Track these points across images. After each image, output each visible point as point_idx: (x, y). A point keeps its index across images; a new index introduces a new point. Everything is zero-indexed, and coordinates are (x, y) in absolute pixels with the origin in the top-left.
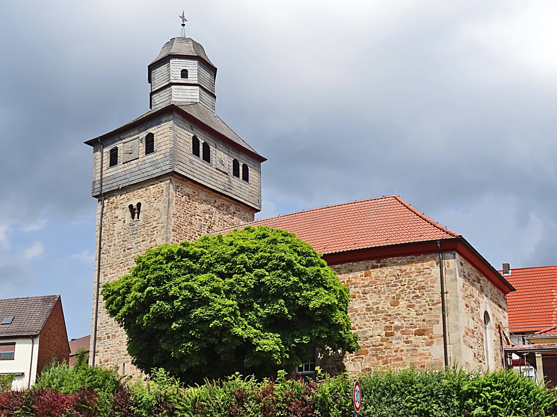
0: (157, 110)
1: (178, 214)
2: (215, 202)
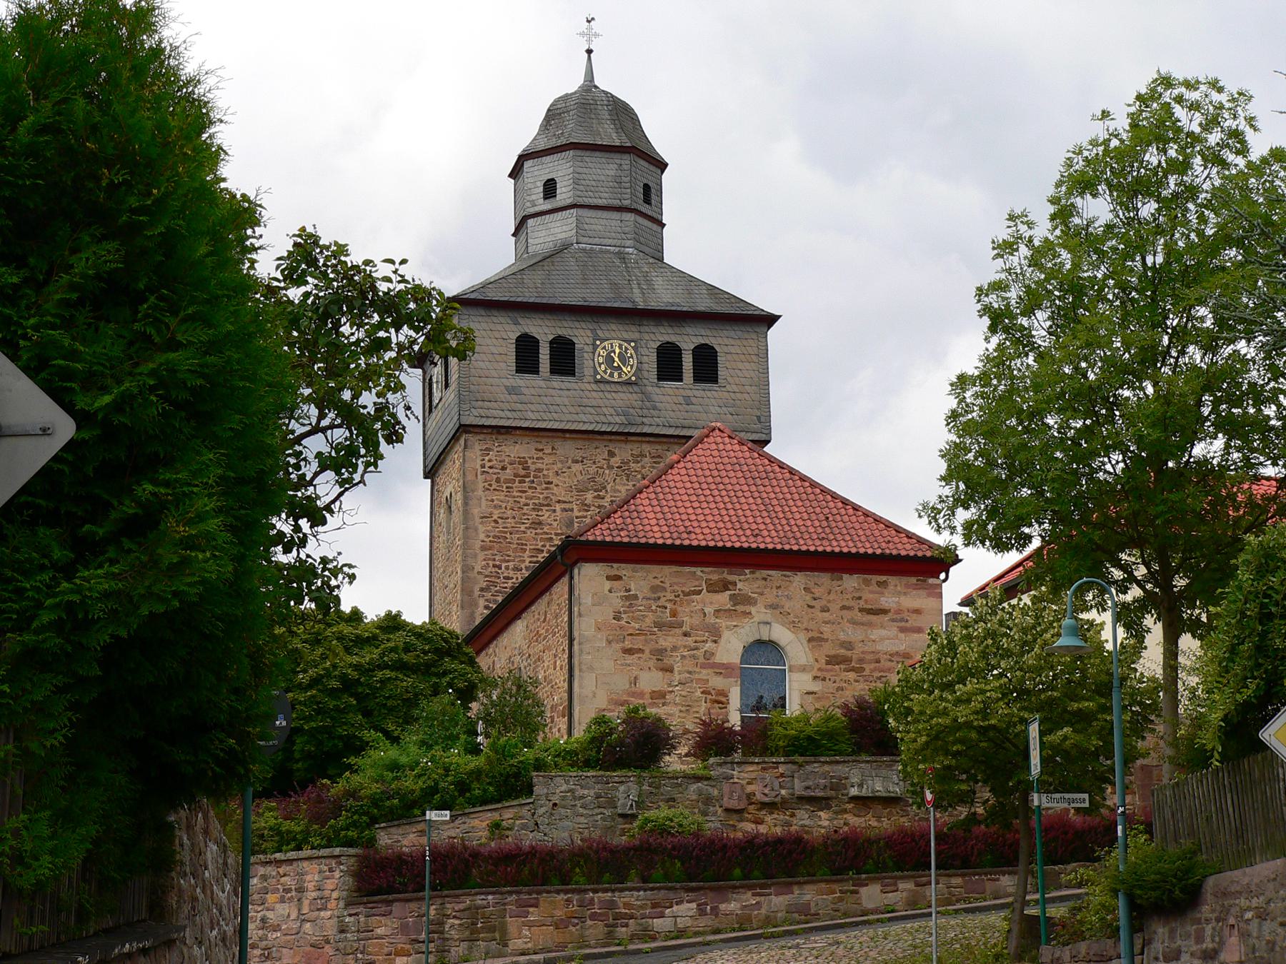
0: (679, 309)
1: (496, 512)
2: (612, 454)
